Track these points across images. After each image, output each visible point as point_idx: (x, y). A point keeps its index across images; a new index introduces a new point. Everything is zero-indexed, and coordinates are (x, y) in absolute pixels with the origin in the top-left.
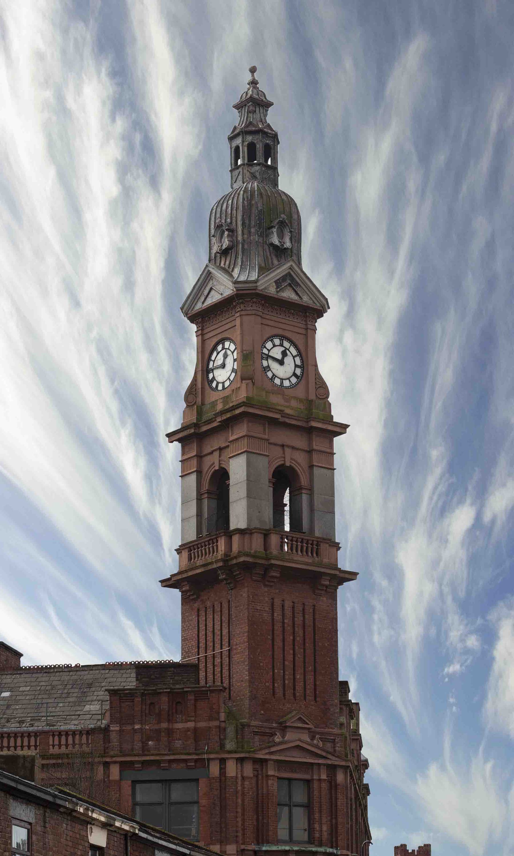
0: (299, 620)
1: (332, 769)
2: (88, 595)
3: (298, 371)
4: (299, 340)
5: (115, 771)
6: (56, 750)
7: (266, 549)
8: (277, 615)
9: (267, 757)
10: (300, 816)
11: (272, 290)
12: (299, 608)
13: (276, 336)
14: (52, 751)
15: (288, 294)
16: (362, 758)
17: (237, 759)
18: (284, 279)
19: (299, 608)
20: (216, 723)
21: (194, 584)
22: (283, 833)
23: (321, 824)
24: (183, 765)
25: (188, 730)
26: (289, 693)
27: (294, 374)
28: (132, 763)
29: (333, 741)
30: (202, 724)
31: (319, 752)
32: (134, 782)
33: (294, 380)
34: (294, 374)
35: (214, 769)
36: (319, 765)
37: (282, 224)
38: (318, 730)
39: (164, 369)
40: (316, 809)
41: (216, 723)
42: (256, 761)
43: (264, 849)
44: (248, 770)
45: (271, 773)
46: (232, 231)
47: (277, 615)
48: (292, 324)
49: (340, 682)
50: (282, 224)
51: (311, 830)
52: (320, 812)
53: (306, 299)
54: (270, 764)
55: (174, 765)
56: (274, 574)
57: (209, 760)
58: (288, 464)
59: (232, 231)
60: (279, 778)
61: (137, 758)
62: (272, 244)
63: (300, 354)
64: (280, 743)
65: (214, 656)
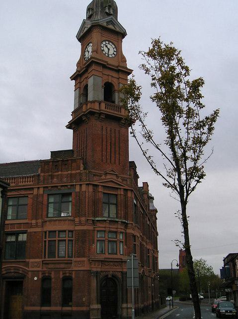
0: (113, 135)
1: (126, 190)
2: (43, 133)
3: (115, 53)
4: (115, 43)
5: (41, 191)
6: (21, 184)
7: (99, 108)
8: (104, 133)
9: (98, 184)
10: (113, 209)
11: (105, 24)
12: (113, 131)
13: (107, 40)
14: (20, 184)
15: (111, 27)
16: (151, 208)
17: (86, 184)
18: (110, 21)
19: (113, 131)
20: (79, 171)
21: (75, 124)
22: (106, 214)
23: (121, 211)
24: (66, 187)
25: (69, 174)
26: (109, 161)
27: (114, 54)
28: (47, 187)
29: (127, 180)
30: (73, 172)
31: (120, 184)
32: (48, 195)
33: (113, 55)
34: (114, 54)
35: (78, 189)
36: (120, 188)
37: (110, 7)
38: (120, 176)
39: (72, 54)
40: (119, 206)
41: (79, 171)
42: (94, 185)
43: (96, 219)
44: (91, 188)
45: (100, 190)
46: (92, 9)
47: (104, 133)
48: (113, 37)
49: (130, 162)
50: (110, 7)
51: (117, 213)
52: (121, 206)
53: (118, 29)
54: (100, 187)
55: (63, 188)
56: (102, 117)
57: (75, 185)
58: (110, 81)
59: (92, 9)
60: (104, 193)
61: (50, 185)
62: (106, 13)
63: (116, 47)
64: (104, 179)
65: (82, 149)
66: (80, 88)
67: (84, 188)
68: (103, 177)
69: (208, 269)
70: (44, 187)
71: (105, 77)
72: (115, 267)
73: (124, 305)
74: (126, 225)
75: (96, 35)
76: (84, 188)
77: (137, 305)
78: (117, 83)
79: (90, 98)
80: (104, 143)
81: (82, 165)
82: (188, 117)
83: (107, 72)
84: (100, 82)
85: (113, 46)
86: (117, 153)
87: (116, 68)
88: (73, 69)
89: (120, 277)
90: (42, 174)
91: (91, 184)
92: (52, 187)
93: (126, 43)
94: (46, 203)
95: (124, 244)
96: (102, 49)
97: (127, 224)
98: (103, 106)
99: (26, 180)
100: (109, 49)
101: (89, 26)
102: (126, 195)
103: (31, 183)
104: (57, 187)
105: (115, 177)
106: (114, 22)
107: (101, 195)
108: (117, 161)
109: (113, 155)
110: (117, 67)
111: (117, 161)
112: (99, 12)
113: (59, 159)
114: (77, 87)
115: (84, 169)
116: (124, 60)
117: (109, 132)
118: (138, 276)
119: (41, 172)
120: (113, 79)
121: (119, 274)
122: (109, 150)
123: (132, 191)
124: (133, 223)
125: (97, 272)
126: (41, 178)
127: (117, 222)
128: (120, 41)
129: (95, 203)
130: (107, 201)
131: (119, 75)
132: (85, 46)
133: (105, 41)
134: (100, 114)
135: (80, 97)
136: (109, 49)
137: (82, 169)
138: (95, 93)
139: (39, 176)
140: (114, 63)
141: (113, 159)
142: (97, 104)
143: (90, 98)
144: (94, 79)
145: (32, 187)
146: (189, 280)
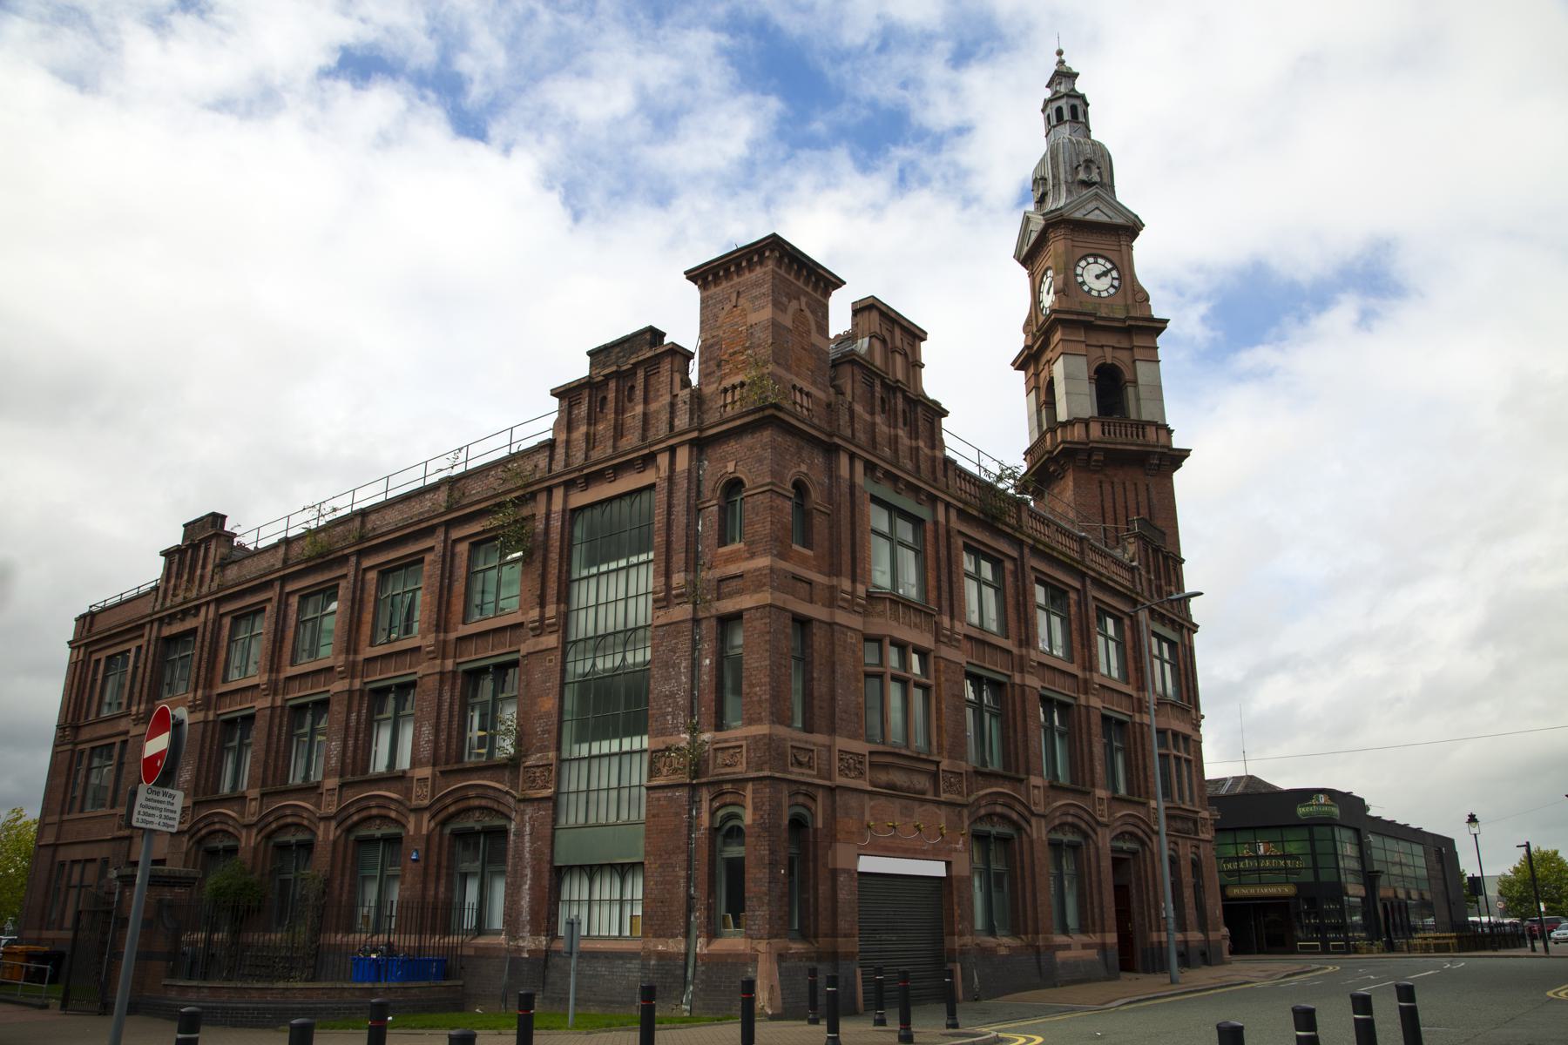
3: (1116, 283)
33: (1112, 291)
69: (507, 150)
71: (1098, 352)
75: (1057, 245)
78: (1128, 362)
79: (1062, 416)
82: (589, 424)
84: (1082, 367)
87: (823, 437)
88: (1017, 342)
93: (1143, 251)
98: (1095, 431)
100: (1095, 278)
114: (1032, 387)
120: (1119, 354)
128: (1124, 248)
133: (1084, 257)
135: (1039, 412)
136: (1095, 278)
138: (1074, 397)
146: (1313, 877)
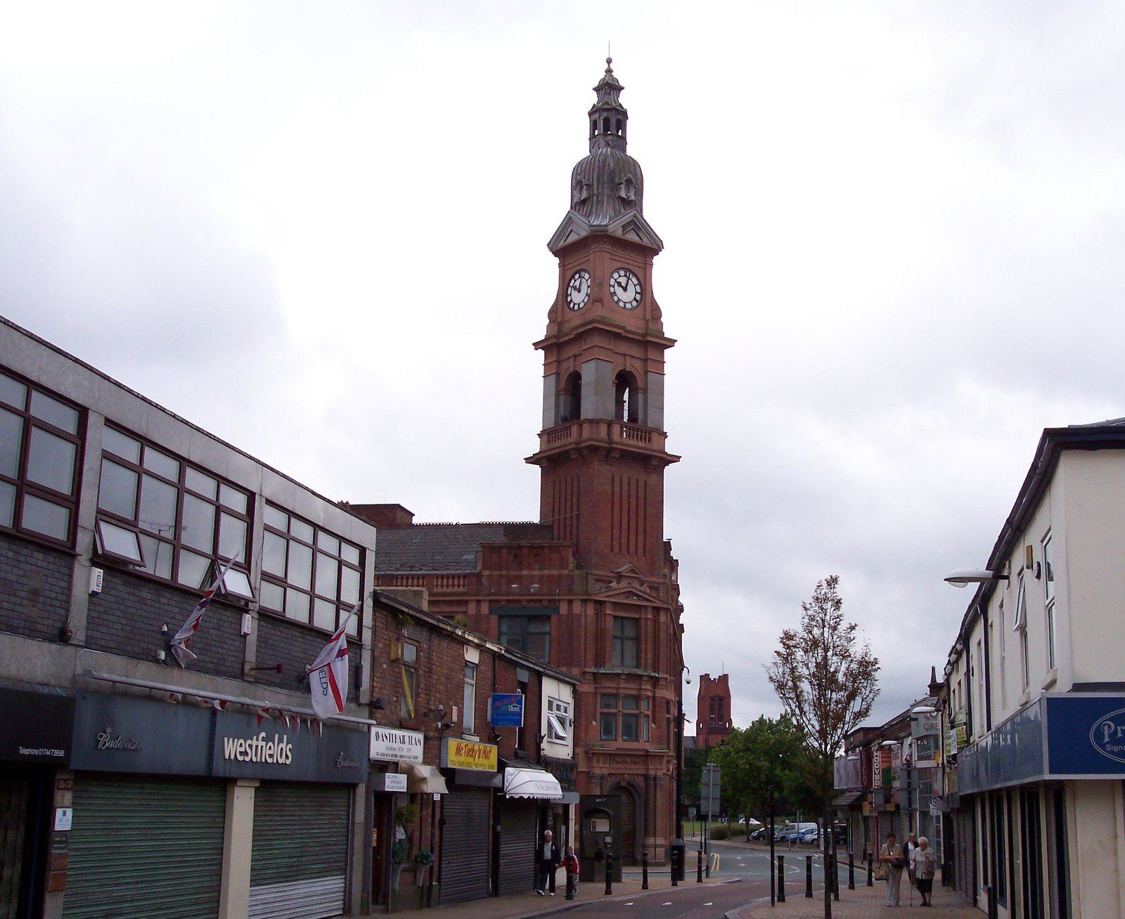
1: (657, 610)
3: (638, 297)
5: (485, 608)
11: (619, 233)
12: (633, 483)
15: (632, 237)
18: (629, 224)
19: (633, 483)
20: (566, 572)
26: (624, 549)
27: (635, 299)
33: (634, 303)
34: (635, 299)
36: (646, 607)
44: (591, 610)
48: (634, 259)
54: (608, 605)
62: (621, 198)
66: (558, 374)
67: (577, 608)
68: (614, 585)
70: (490, 601)
72: (633, 766)
73: (651, 841)
74: (655, 682)
76: (577, 608)
77: (668, 840)
78: (642, 372)
80: (617, 510)
81: (571, 559)
83: (623, 348)
84: (610, 373)
85: (638, 287)
86: (641, 530)
89: (642, 784)
90: (486, 573)
91: (590, 600)
92: (508, 601)
94: (497, 633)
95: (650, 720)
96: (612, 290)
97: (658, 678)
99: (439, 583)
101: (583, 234)
102: (656, 621)
103: (461, 589)
104: (519, 601)
105: (636, 584)
106: (638, 225)
107: (609, 622)
108: (640, 549)
109: (632, 536)
110: (645, 335)
111: (640, 549)
112: (605, 199)
113: (523, 543)
115: (579, 567)
116: (656, 312)
117: (625, 487)
118: (719, 797)
119: (484, 568)
121: (641, 779)
122: (625, 526)
123: (668, 610)
124: (667, 676)
125: (602, 777)
126: (485, 581)
127: (641, 676)
129: (600, 636)
130: (618, 634)
131: (646, 351)
132: (570, 273)
133: (617, 270)
134: (610, 450)
137: (571, 567)
139: (479, 575)
140: (633, 325)
141: (632, 545)
142: (603, 429)
143: (588, 409)
144: (597, 368)
145: (465, 598)
